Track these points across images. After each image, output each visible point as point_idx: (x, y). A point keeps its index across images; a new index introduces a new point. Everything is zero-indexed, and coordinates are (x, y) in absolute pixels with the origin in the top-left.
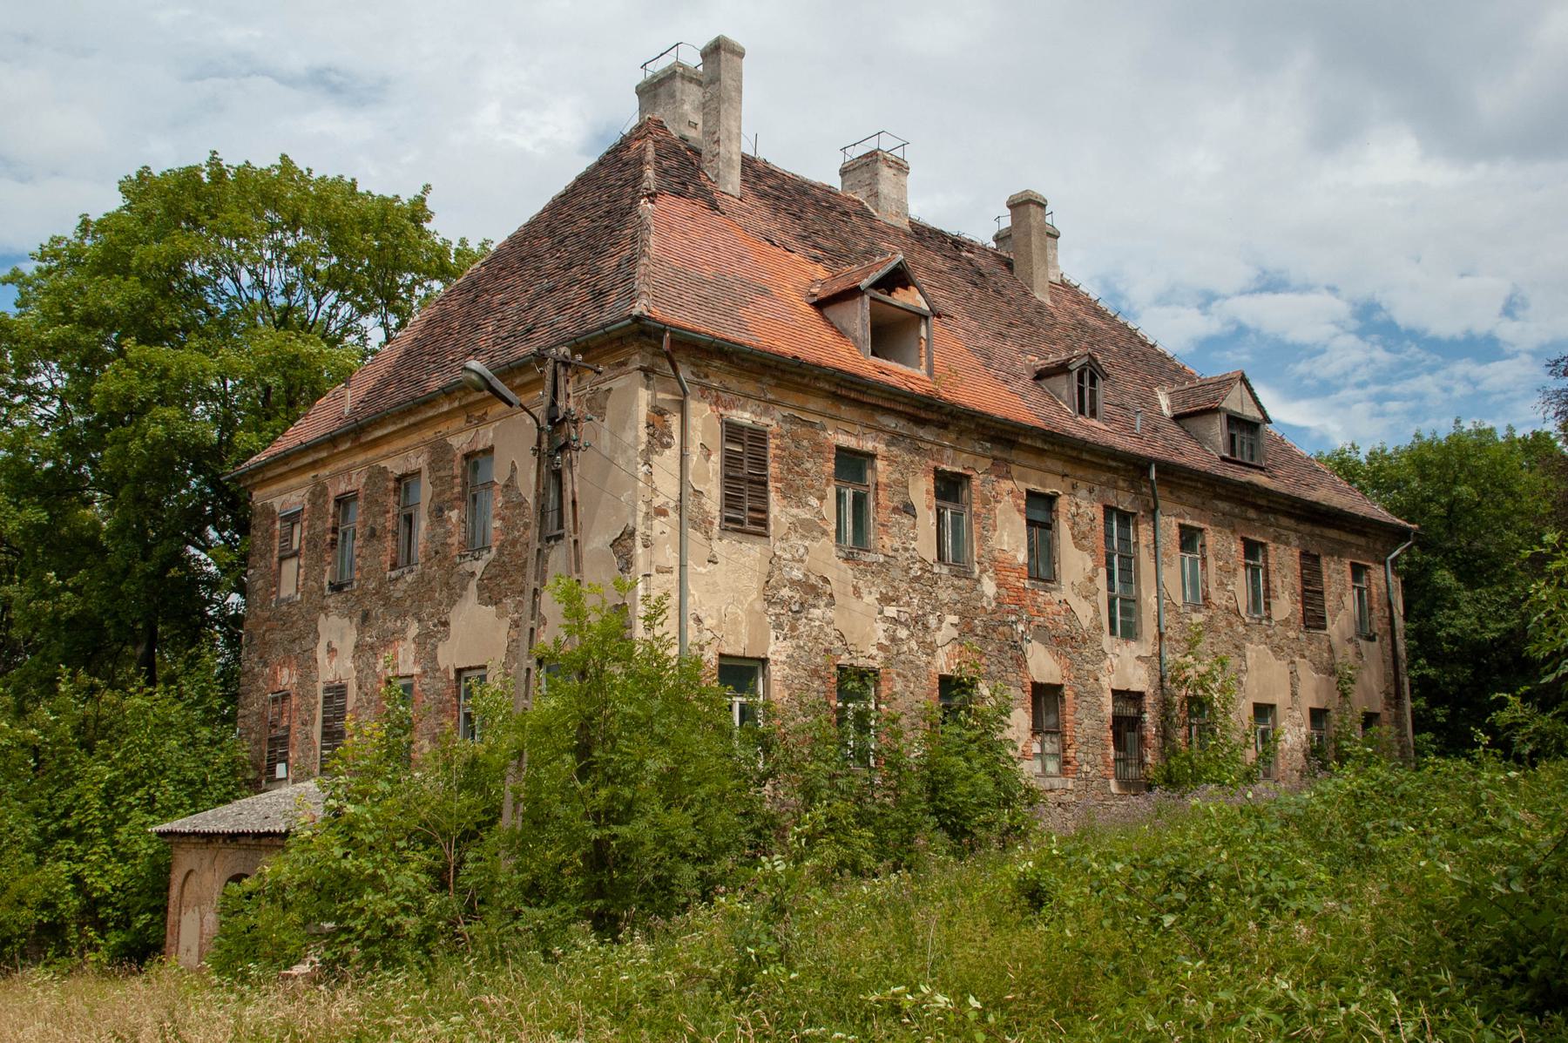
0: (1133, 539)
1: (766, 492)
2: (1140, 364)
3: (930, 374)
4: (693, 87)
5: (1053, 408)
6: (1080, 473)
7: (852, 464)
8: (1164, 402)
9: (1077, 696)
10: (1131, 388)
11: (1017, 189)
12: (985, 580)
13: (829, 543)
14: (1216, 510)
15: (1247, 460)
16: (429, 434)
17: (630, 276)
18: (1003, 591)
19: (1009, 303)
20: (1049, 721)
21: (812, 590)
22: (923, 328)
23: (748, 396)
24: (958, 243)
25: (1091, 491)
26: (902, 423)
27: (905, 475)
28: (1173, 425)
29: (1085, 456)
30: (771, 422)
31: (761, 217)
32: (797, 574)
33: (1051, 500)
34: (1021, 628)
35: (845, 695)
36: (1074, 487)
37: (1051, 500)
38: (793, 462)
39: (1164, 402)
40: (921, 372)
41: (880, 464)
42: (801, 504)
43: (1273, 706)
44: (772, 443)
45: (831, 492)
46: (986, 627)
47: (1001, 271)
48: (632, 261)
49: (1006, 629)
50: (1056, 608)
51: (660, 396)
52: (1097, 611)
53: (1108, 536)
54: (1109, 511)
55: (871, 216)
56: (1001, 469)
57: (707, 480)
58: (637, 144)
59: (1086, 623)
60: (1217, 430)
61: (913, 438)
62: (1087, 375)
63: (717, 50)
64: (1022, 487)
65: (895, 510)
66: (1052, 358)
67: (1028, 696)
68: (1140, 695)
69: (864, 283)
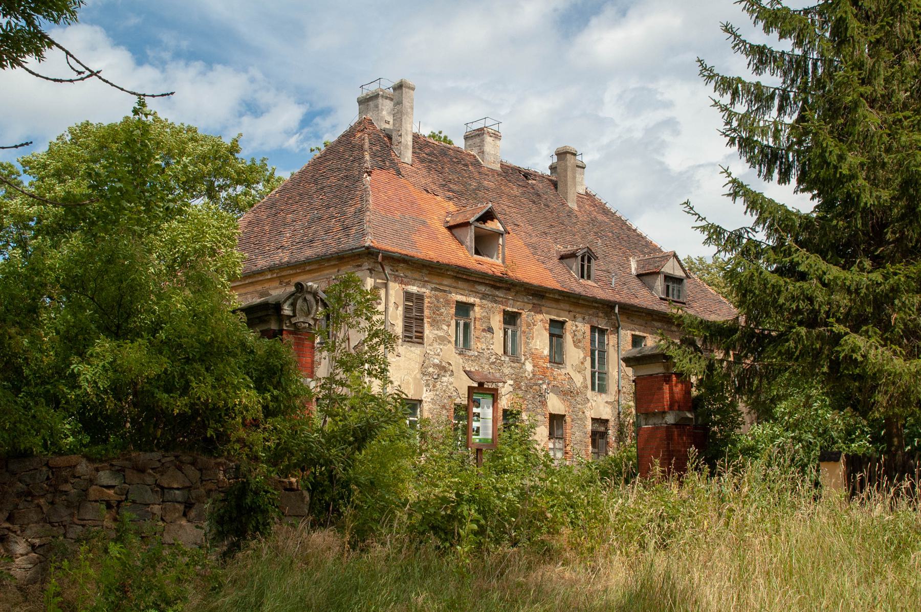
0: (606, 342)
1: (423, 323)
2: (624, 243)
3: (504, 262)
4: (388, 101)
5: (567, 276)
6: (578, 310)
7: (463, 309)
8: (633, 265)
9: (573, 421)
10: (615, 259)
11: (560, 145)
12: (527, 363)
13: (451, 347)
14: (654, 326)
15: (675, 299)
16: (259, 288)
17: (360, 222)
18: (536, 369)
19: (552, 212)
20: (557, 433)
21: (443, 369)
22: (501, 239)
23: (415, 279)
24: (527, 175)
25: (584, 319)
26: (488, 288)
27: (488, 313)
28: (637, 281)
29: (581, 302)
30: (426, 291)
31: (423, 177)
32: (437, 361)
33: (563, 323)
34: (545, 386)
35: (459, 418)
36: (575, 317)
37: (563, 323)
38: (436, 309)
39: (633, 265)
40: (499, 262)
41: (477, 309)
42: (439, 329)
43: (421, 401)
44: (426, 300)
45: (453, 323)
46: (527, 386)
47: (551, 191)
48: (361, 211)
49: (537, 387)
50: (563, 377)
51: (378, 281)
52: (585, 379)
53: (593, 341)
54: (593, 329)
55: (480, 165)
56: (537, 309)
57: (397, 319)
58: (359, 135)
59: (579, 385)
60: (659, 283)
61: (494, 296)
62: (586, 258)
63: (399, 87)
64: (548, 317)
65: (484, 330)
66: (569, 248)
67: (547, 420)
68: (607, 421)
69: (472, 220)
